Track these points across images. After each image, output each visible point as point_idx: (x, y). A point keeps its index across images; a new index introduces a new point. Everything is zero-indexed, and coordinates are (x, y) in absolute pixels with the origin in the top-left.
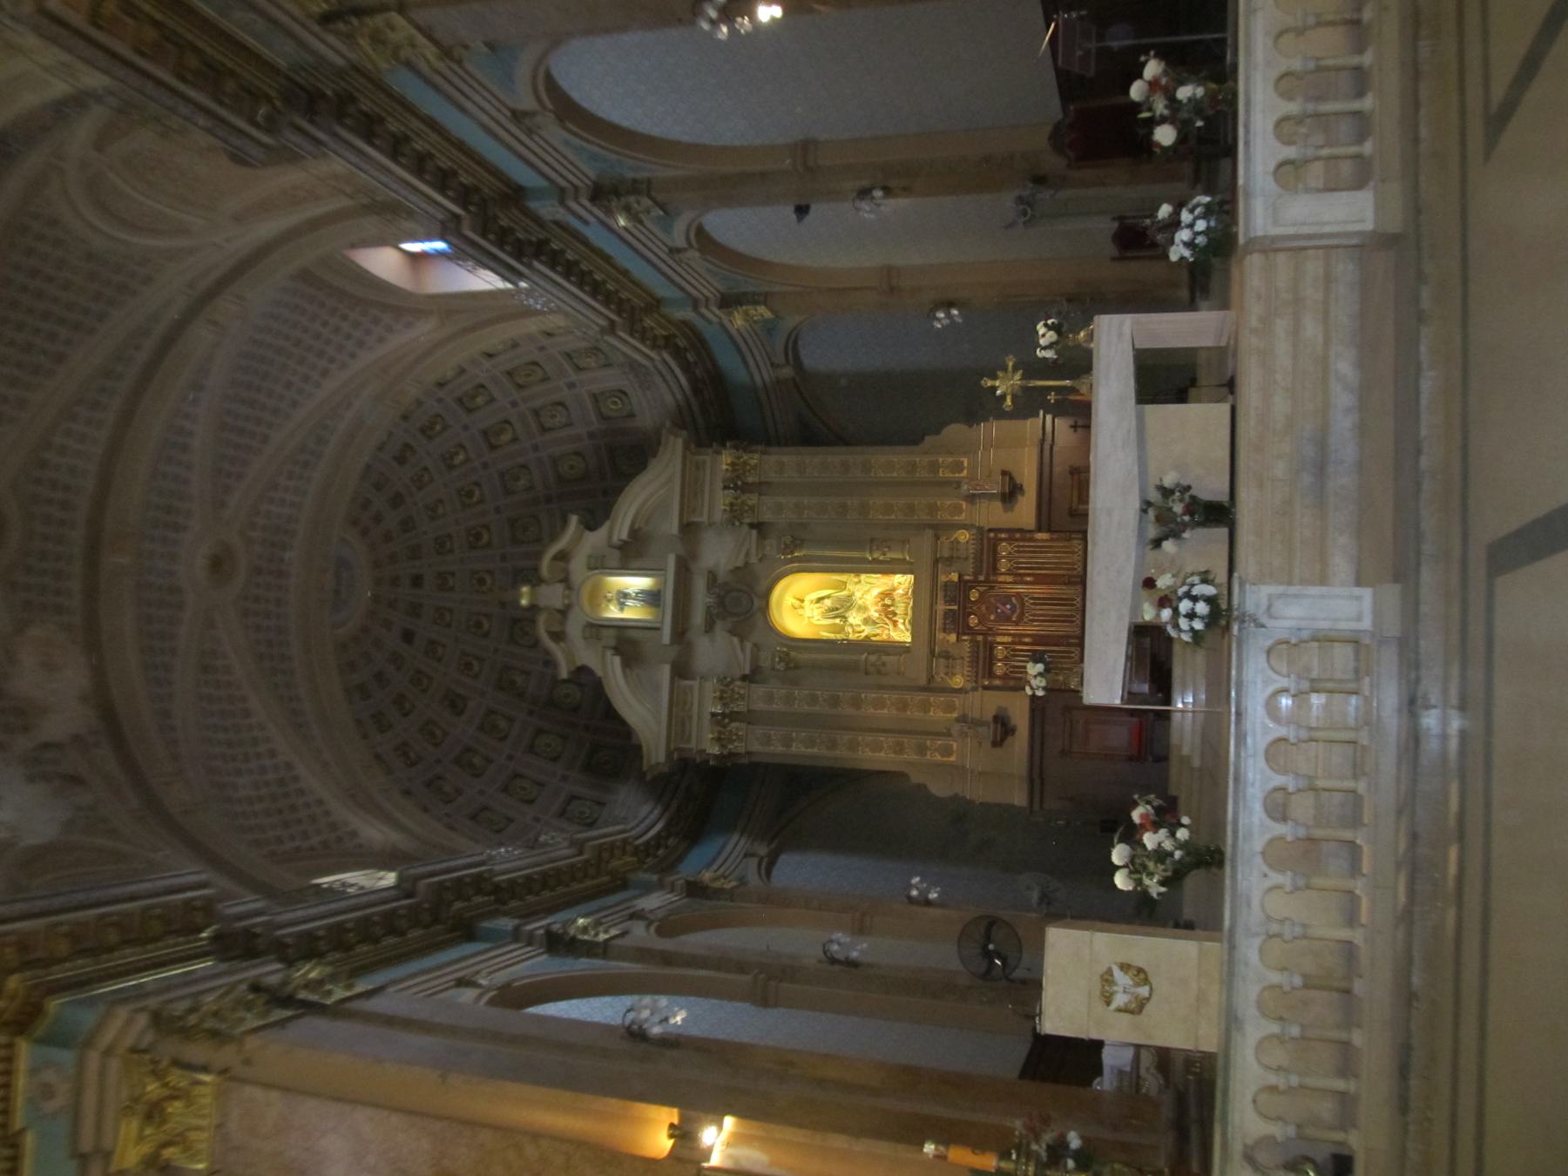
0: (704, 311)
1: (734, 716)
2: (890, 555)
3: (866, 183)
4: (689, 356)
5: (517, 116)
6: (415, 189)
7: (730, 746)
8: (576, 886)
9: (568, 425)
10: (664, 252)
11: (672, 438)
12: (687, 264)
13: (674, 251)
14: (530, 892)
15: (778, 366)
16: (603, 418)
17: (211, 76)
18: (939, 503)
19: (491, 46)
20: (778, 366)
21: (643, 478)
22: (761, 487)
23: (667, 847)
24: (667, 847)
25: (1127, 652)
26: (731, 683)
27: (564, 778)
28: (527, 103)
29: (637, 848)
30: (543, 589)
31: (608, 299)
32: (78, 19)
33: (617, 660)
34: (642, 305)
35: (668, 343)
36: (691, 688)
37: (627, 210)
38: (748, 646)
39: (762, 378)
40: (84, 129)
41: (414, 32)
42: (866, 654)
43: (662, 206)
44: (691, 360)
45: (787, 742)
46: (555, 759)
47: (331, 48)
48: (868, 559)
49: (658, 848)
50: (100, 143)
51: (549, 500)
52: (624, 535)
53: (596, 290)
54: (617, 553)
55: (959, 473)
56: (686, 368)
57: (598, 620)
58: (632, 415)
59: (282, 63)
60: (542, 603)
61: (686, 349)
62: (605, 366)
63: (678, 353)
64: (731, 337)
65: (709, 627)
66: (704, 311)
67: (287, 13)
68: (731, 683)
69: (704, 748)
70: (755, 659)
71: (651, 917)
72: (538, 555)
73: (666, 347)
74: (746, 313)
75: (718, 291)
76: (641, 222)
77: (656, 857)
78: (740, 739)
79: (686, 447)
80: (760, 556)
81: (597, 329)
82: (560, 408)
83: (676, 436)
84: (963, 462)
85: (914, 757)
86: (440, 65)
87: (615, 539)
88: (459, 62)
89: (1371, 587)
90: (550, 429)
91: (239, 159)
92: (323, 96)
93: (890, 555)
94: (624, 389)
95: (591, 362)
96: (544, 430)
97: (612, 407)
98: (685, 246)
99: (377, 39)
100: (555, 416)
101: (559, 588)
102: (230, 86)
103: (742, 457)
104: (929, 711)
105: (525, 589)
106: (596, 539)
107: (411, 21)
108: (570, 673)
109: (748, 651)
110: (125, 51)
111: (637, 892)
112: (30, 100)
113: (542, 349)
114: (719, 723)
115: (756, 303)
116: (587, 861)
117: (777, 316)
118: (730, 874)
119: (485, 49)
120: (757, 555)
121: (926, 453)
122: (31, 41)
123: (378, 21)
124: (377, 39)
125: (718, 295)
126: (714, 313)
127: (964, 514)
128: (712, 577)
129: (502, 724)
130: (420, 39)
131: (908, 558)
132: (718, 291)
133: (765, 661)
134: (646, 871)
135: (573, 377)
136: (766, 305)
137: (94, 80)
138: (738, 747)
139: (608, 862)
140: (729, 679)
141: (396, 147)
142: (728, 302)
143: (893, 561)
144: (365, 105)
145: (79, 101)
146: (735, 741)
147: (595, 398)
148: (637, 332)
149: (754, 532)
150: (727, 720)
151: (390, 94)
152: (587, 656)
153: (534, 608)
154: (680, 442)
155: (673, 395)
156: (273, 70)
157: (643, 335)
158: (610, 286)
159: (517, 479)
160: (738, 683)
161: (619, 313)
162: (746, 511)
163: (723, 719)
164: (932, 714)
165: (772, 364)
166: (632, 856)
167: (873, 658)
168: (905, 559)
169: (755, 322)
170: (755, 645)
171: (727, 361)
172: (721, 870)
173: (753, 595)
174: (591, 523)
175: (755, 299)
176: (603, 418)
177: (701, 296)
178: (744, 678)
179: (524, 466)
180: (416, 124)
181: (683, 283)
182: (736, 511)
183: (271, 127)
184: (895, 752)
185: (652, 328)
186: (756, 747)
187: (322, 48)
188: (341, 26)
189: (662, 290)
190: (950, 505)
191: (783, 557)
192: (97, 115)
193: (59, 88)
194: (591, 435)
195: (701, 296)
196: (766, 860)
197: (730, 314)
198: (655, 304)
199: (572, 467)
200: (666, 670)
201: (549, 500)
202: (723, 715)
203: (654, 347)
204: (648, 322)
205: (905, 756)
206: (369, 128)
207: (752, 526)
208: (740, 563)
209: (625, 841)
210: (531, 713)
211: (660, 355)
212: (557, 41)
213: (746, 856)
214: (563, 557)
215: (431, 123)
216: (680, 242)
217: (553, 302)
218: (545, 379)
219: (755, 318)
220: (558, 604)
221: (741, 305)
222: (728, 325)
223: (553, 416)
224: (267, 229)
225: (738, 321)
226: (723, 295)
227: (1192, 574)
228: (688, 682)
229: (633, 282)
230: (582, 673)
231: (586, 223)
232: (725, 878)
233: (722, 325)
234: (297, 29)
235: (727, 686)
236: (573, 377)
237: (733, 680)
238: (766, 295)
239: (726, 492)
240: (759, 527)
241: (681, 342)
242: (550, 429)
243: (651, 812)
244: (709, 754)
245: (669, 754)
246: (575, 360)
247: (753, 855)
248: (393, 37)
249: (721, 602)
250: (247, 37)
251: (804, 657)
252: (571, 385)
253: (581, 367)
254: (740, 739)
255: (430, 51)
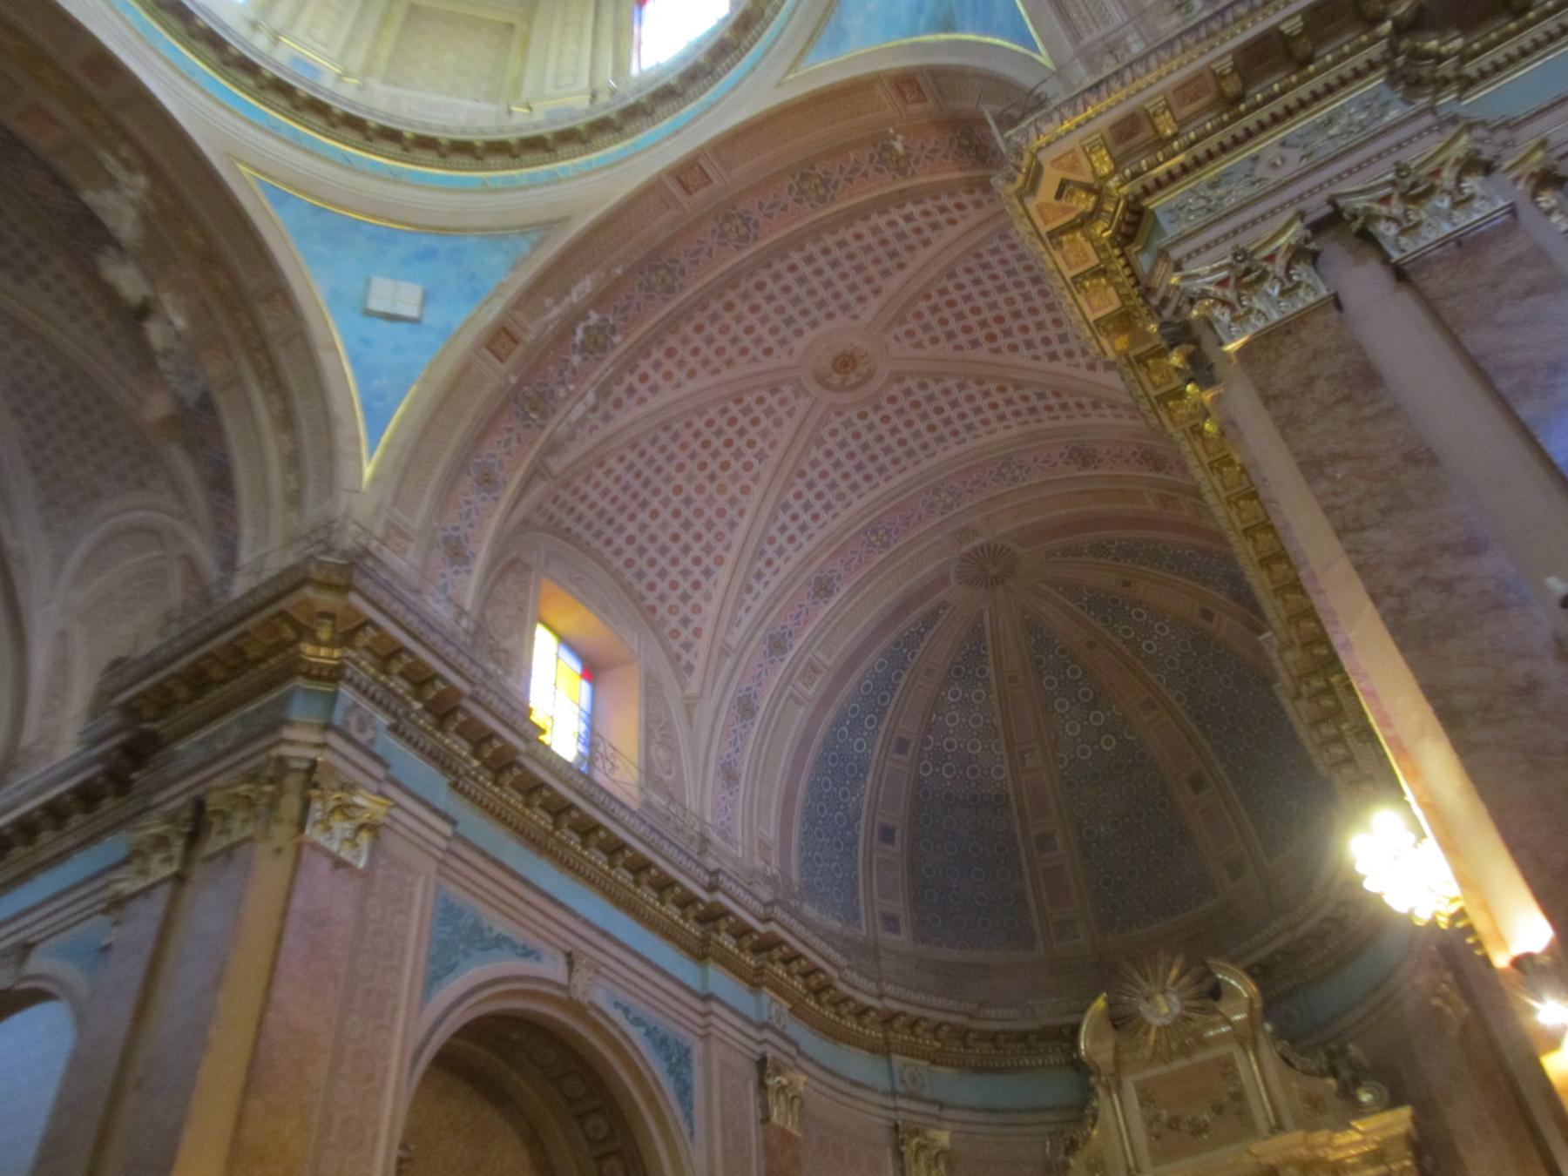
5: (26, 948)
6: (409, 632)
17: (198, 681)
19: (107, 949)
28: (38, 963)
32: (286, 604)
40: (207, 559)
41: (151, 880)
47: (174, 797)
50: (189, 562)
59: (181, 746)
67: (217, 775)
86: (108, 893)
88: (105, 912)
90: (1278, 1118)
91: (118, 664)
92: (137, 769)
99: (161, 842)
102: (182, 692)
107: (163, 881)
110: (250, 624)
112: (247, 531)
119: (105, 942)
122: (290, 559)
123: (178, 848)
124: (161, 842)
130: (141, 883)
137: (241, 586)
141: (55, 813)
144: (108, 804)
145: (229, 564)
151: (107, 831)
156: (180, 736)
180: (70, 842)
183: (129, 710)
187: (174, 790)
188: (187, 814)
192: (212, 571)
193: (246, 557)
206: (87, 796)
212: (81, 1017)
215: (61, 857)
217: (1342, 45)
224: (41, 656)
234: (197, 778)
242: (1278, 1118)
248: (158, 857)
250: (219, 726)
255: (127, 887)
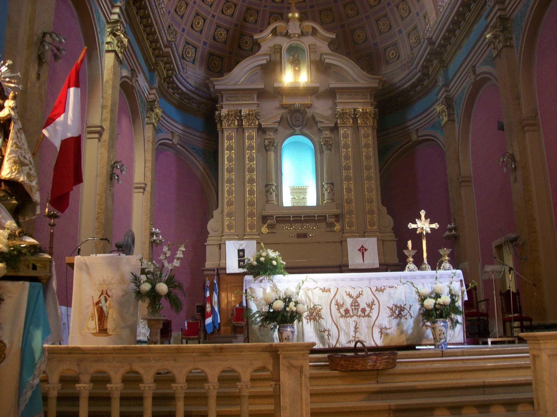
0: (443, 90)
1: (240, 121)
2: (326, 193)
3: (518, 158)
4: (420, 87)
7: (225, 120)
8: (148, 44)
9: (380, 33)
10: (473, 64)
11: (378, 81)
12: (468, 76)
13: (474, 67)
14: (141, 18)
15: (417, 133)
16: (386, 49)
18: (353, 216)
20: (417, 133)
21: (358, 69)
22: (356, 127)
23: (174, 94)
24: (174, 94)
25: (139, 48)
26: (257, 118)
27: (205, 43)
29: (171, 77)
30: (298, 23)
31: (446, 39)
33: (265, 62)
34: (444, 59)
35: (425, 75)
36: (254, 100)
37: (495, 37)
38: (276, 126)
39: (410, 126)
42: (276, 184)
43: (498, 55)
44: (417, 89)
45: (230, 148)
46: (214, 38)
48: (323, 182)
49: (172, 89)
51: (343, 26)
52: (327, 61)
53: (451, 31)
54: (318, 59)
55: (369, 225)
56: (414, 86)
57: (284, 66)
58: (387, 63)
60: (291, 24)
61: (423, 85)
62: (411, 47)
63: (420, 81)
64: (430, 107)
65: (283, 107)
66: (443, 90)
68: (257, 118)
69: (223, 108)
70: (270, 129)
71: (134, 80)
72: (314, 20)
73: (424, 74)
74: (443, 111)
75: (454, 96)
76: (489, 46)
77: (168, 88)
78: (230, 125)
79: (373, 89)
80: (321, 129)
81: (430, 36)
82: (388, 27)
83: (379, 83)
84: (375, 226)
85: (226, 212)
87: (325, 57)
89: (275, 87)
93: (326, 193)
94: (400, 58)
95: (413, 40)
96: (377, 21)
97: (391, 53)
98: (477, 73)
100: (384, 26)
101: (299, 32)
103: (370, 117)
104: (249, 217)
105: (297, 15)
106: (324, 47)
108: (257, 40)
109: (274, 126)
111: (148, 78)
113: (418, 14)
114: (236, 113)
115: (449, 115)
116: (161, 49)
117: (442, 128)
118: (160, 123)
120: (321, 127)
121: (378, 209)
125: (451, 97)
126: (442, 95)
127: (348, 228)
128: (310, 106)
129: (229, 12)
131: (325, 202)
132: (454, 96)
133: (270, 135)
134: (160, 82)
135: (405, 32)
136: (448, 120)
138: (225, 124)
139: (162, 61)
140: (258, 117)
142: (449, 103)
143: (323, 195)
146: (228, 123)
147: (395, 44)
148: (430, 57)
149: (333, 125)
150: (238, 118)
152: (265, 47)
153: (288, 20)
154: (376, 85)
155: (399, 82)
157: (429, 61)
158: (453, 40)
159: (351, 10)
160: (257, 123)
161: (440, 46)
162: (343, 121)
163: (238, 116)
164: (248, 219)
165: (417, 130)
166: (167, 74)
167: (274, 188)
168: (324, 201)
169: (439, 117)
170: (277, 130)
171: (418, 107)
172: (161, 118)
173: (301, 127)
174: (331, 44)
175: (451, 116)
176: (386, 49)
177: (450, 88)
178: (260, 125)
179: (358, 13)
181: (456, 78)
182: (343, 115)
184: (228, 202)
185: (432, 65)
186: (226, 134)
189: (452, 69)
190: (353, 222)
191: (321, 140)
194: (376, 45)
195: (450, 88)
196: (171, 142)
197: (442, 104)
198: (444, 65)
199: (359, 36)
200: (261, 86)
201: (343, 26)
202: (241, 116)
203: (423, 67)
204: (435, 62)
205: (226, 207)
207: (336, 124)
208: (317, 119)
209: (173, 70)
210: (236, 25)
211: (419, 71)
213: (172, 132)
214: (314, 32)
216: (478, 71)
218: (402, 18)
219: (441, 117)
220: (290, 32)
221: (447, 108)
222: (437, 104)
223: (384, 24)
225: (439, 108)
226: (452, 99)
227: (340, 312)
228: (256, 96)
229: (455, 52)
230: (257, 45)
231: (486, 19)
232: (158, 120)
233: (437, 100)
235: (255, 117)
236: (405, 32)
237: (258, 119)
238: (453, 120)
239: (352, 110)
240: (335, 129)
241: (426, 82)
243: (190, 85)
244: (221, 111)
245: (220, 91)
246: (413, 32)
247: (172, 136)
249: (297, 111)
251: (272, 154)
252: (400, 32)
253: (410, 36)
254: (230, 125)
